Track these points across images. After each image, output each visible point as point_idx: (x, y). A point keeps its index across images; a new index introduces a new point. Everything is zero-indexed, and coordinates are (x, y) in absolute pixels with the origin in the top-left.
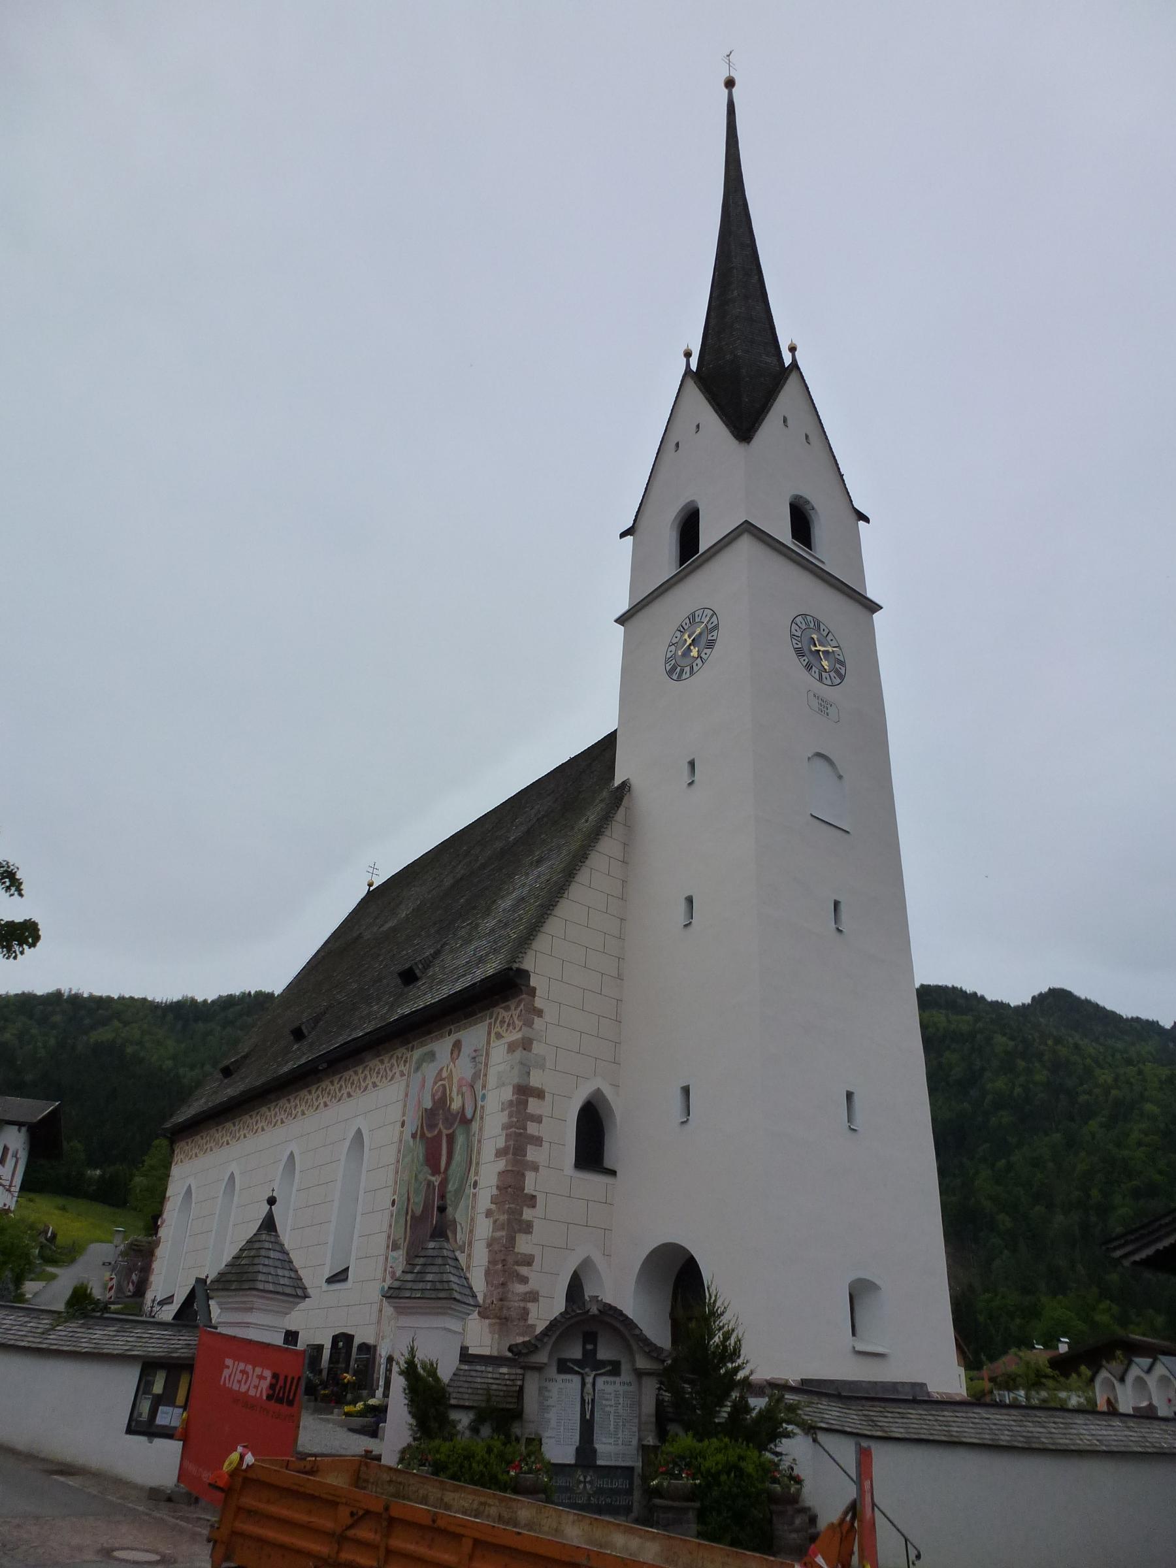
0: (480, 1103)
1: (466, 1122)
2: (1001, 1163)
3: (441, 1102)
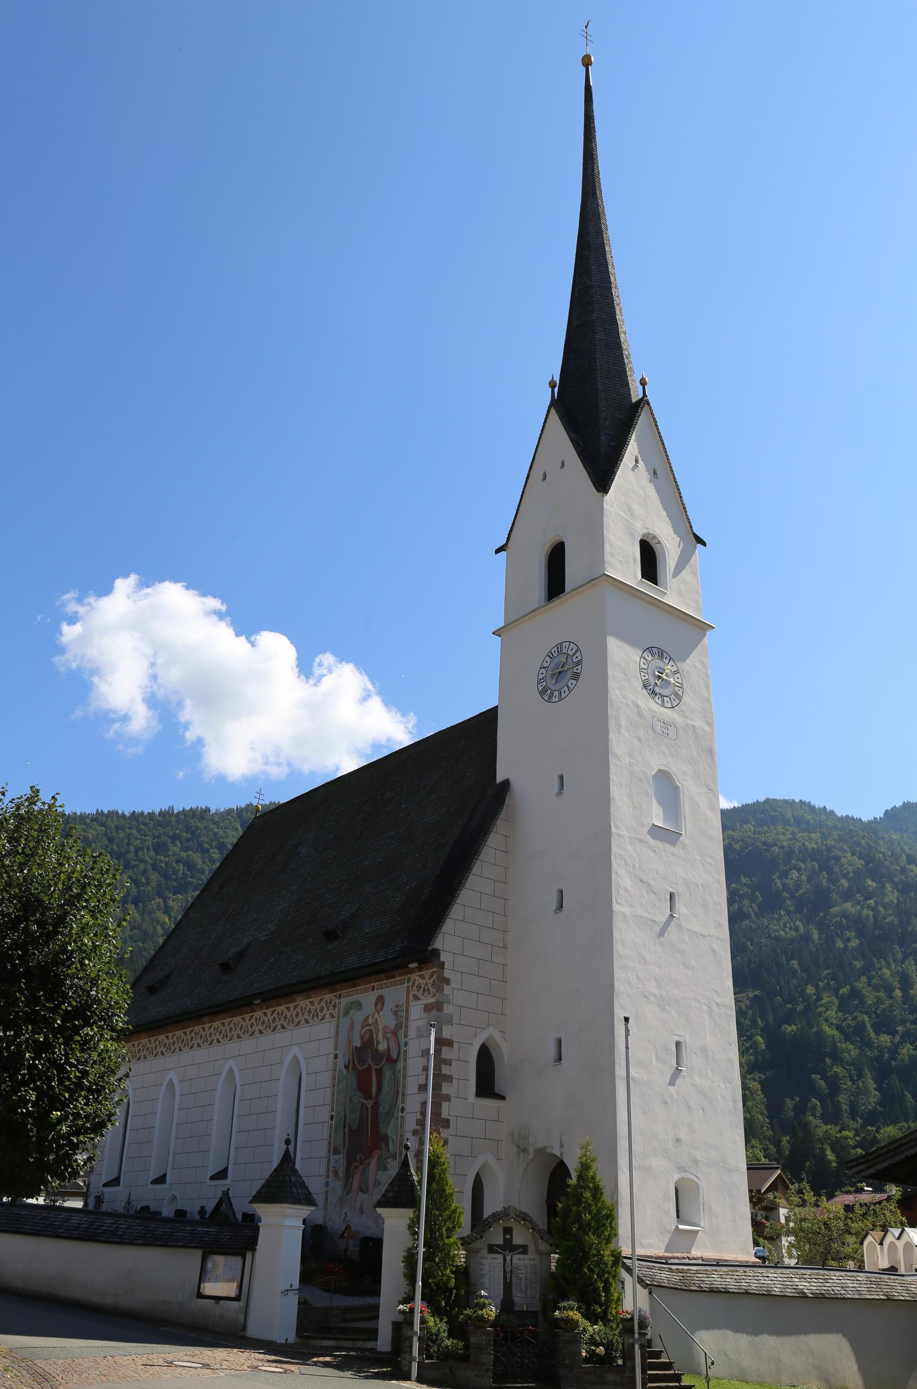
0: (403, 1048)
1: (392, 1061)
2: (845, 990)
3: (369, 1043)
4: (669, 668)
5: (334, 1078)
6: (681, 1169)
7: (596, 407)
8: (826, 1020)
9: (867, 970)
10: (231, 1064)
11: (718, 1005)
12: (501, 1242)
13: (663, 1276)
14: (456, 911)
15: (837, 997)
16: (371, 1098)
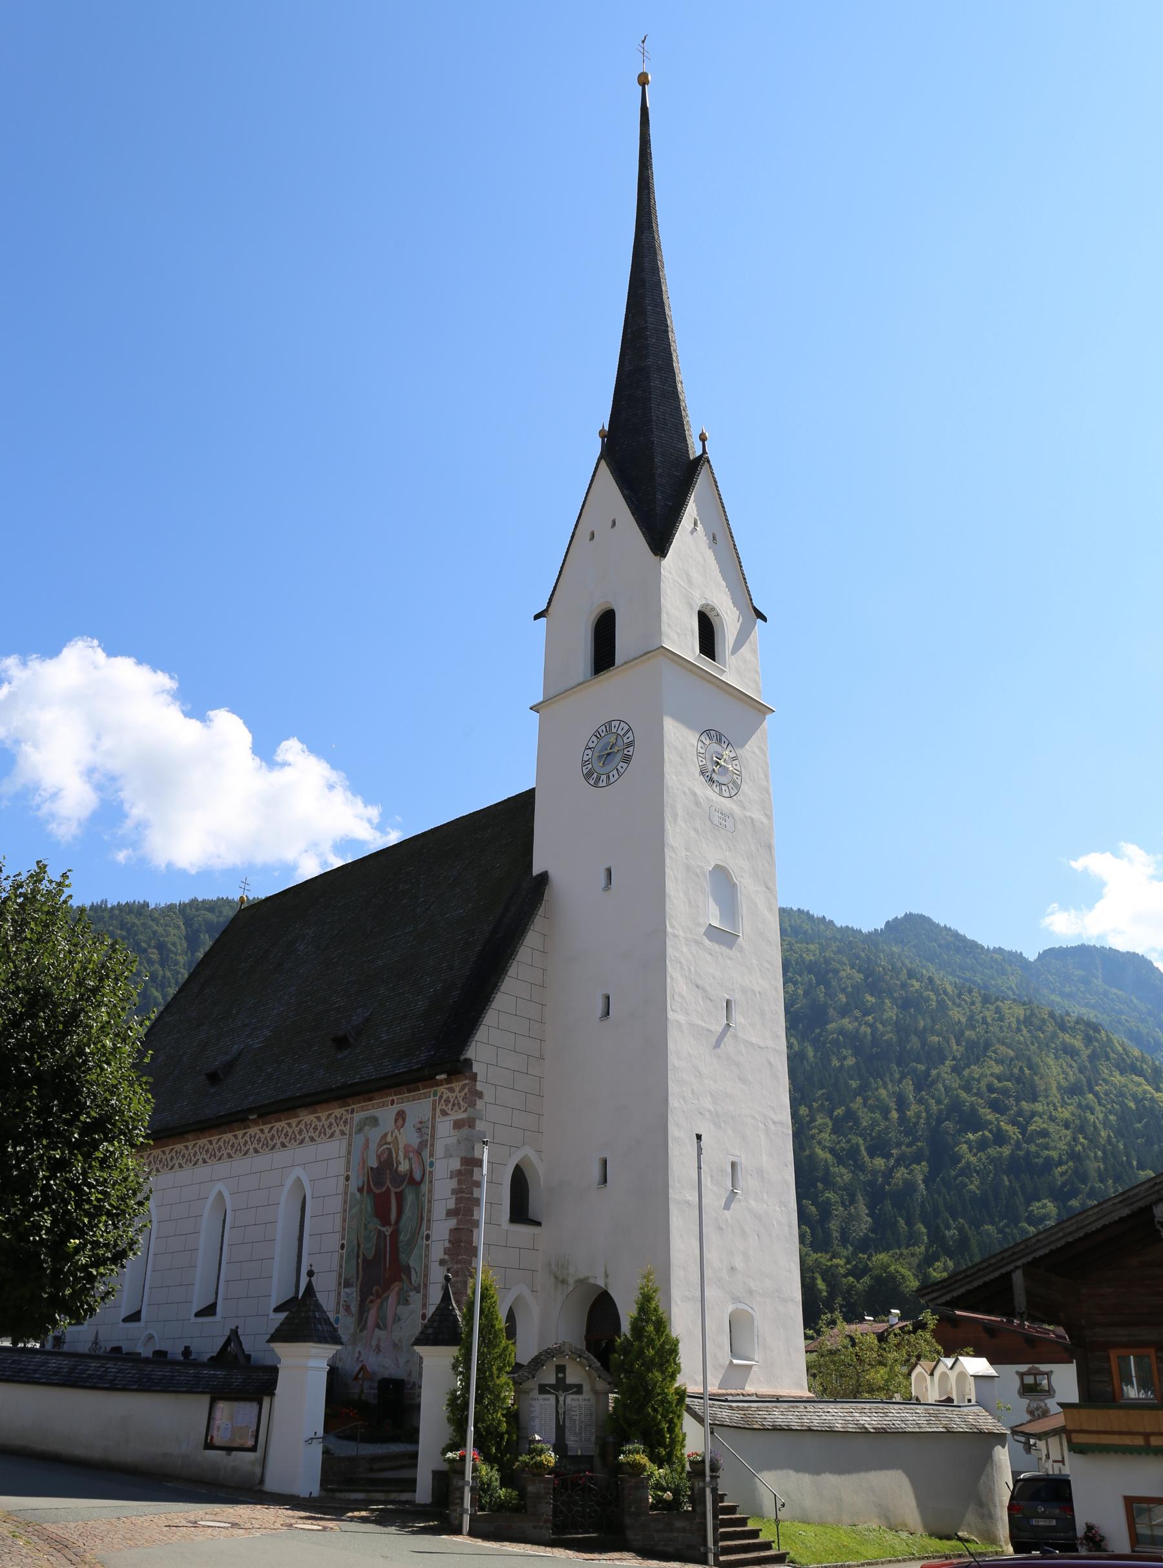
0: (428, 1169)
1: (415, 1184)
2: (839, 1111)
4: (727, 754)
5: (345, 1202)
6: (736, 1299)
7: (650, 460)
8: (819, 1143)
9: (863, 1088)
10: (220, 1186)
11: (774, 1122)
12: (553, 1381)
13: (724, 1415)
14: (490, 1017)
15: (831, 1118)
16: (390, 1224)
